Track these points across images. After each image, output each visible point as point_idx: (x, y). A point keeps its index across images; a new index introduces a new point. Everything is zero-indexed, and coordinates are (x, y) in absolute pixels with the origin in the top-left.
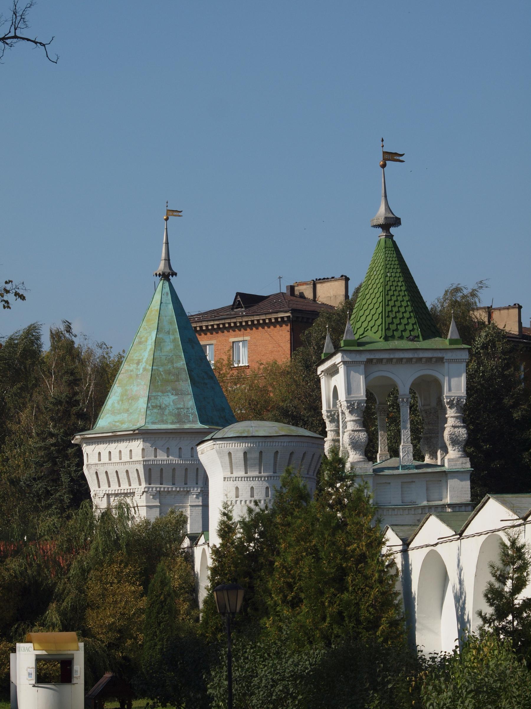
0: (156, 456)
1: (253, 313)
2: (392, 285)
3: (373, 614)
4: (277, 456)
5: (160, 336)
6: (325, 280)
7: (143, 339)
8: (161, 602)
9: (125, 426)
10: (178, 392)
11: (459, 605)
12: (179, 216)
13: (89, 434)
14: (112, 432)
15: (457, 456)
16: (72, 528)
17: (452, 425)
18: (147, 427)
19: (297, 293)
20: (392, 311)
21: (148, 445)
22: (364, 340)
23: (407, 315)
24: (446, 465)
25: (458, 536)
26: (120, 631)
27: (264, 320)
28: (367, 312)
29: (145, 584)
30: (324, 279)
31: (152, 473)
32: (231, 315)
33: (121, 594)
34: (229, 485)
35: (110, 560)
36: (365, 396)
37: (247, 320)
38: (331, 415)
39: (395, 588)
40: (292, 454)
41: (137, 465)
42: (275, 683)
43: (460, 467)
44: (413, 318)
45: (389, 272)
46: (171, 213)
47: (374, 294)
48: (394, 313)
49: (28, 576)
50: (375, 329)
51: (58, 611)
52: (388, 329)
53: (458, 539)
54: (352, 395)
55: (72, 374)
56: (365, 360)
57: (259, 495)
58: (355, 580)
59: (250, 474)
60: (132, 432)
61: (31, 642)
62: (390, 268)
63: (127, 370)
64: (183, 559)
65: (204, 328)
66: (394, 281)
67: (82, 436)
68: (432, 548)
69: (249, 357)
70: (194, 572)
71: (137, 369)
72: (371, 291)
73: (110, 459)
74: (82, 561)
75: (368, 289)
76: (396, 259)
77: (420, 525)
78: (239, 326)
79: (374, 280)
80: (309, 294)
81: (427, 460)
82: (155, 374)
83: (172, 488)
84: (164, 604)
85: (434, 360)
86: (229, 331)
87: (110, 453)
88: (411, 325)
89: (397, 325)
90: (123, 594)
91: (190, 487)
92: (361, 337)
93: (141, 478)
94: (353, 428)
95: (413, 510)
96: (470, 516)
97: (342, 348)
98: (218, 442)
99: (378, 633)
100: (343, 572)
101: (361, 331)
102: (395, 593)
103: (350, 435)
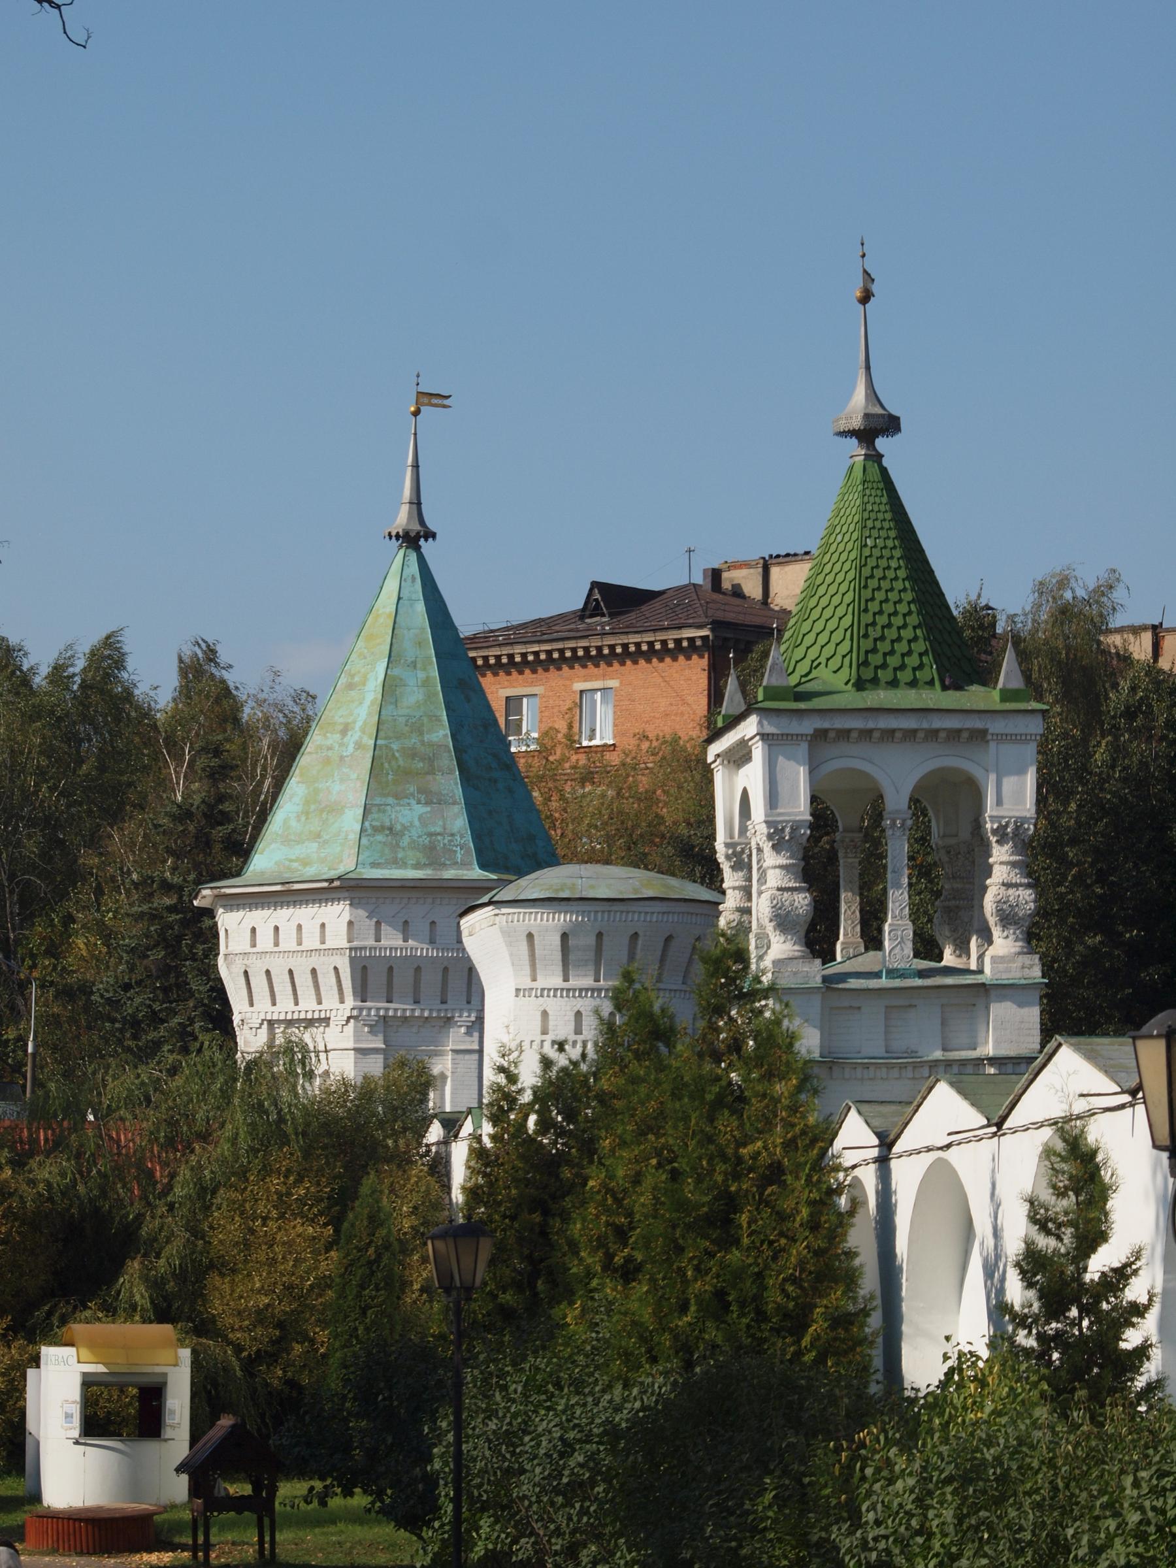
0: (378, 940)
1: (628, 627)
2: (877, 567)
3: (794, 1299)
4: (636, 944)
5: (396, 672)
6: (789, 558)
7: (356, 679)
8: (370, 1263)
9: (310, 871)
10: (430, 798)
11: (992, 1284)
12: (445, 406)
13: (231, 887)
14: (282, 884)
15: (1013, 950)
16: (179, 1096)
17: (1003, 881)
18: (360, 873)
19: (726, 585)
20: (874, 624)
21: (362, 913)
22: (809, 687)
23: (907, 634)
24: (987, 969)
25: (994, 1129)
26: (280, 1325)
27: (651, 644)
28: (819, 626)
29: (336, 1222)
30: (788, 555)
31: (369, 976)
32: (577, 630)
33: (284, 1243)
34: (527, 1003)
35: (264, 1166)
36: (808, 813)
37: (612, 642)
38: (735, 854)
39: (846, 1241)
40: (669, 939)
41: (335, 957)
42: (567, 1449)
43: (1018, 975)
44: (921, 641)
45: (870, 537)
46: (426, 400)
47: (835, 585)
48: (879, 628)
49: (79, 1198)
50: (835, 663)
51: (145, 1278)
52: (866, 663)
53: (995, 1134)
54: (779, 810)
55: (217, 752)
56: (811, 731)
57: (562, 1028)
58: (756, 1221)
59: (573, 982)
60: (325, 884)
61: (72, 1345)
62: (874, 528)
63: (320, 747)
64: (426, 1168)
65: (518, 659)
66: (882, 557)
67: (216, 892)
68: (940, 1154)
69: (615, 725)
70: (451, 1199)
71: (341, 745)
72: (829, 579)
73: (276, 944)
74: (200, 1167)
75: (823, 575)
76: (888, 507)
77: (915, 1103)
78: (596, 656)
79: (837, 554)
80: (753, 589)
81: (949, 958)
82: (380, 757)
83: (413, 1010)
84: (374, 1268)
85: (965, 735)
86: (572, 668)
87: (276, 929)
88: (915, 656)
89: (885, 655)
90: (289, 1244)
91: (453, 1010)
92: (803, 680)
93: (344, 986)
94: (779, 884)
95: (910, 1069)
96: (1020, 1085)
97: (760, 705)
98: (504, 910)
99: (806, 1341)
100: (730, 1204)
101: (803, 668)
102: (845, 1253)
103: (773, 899)
